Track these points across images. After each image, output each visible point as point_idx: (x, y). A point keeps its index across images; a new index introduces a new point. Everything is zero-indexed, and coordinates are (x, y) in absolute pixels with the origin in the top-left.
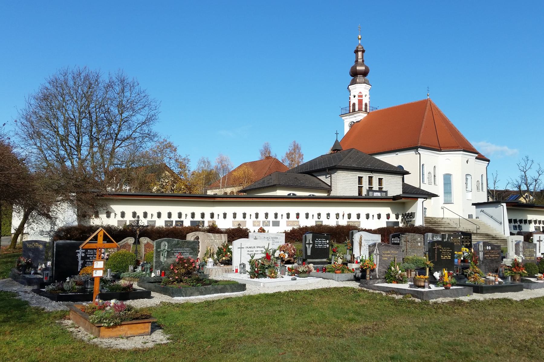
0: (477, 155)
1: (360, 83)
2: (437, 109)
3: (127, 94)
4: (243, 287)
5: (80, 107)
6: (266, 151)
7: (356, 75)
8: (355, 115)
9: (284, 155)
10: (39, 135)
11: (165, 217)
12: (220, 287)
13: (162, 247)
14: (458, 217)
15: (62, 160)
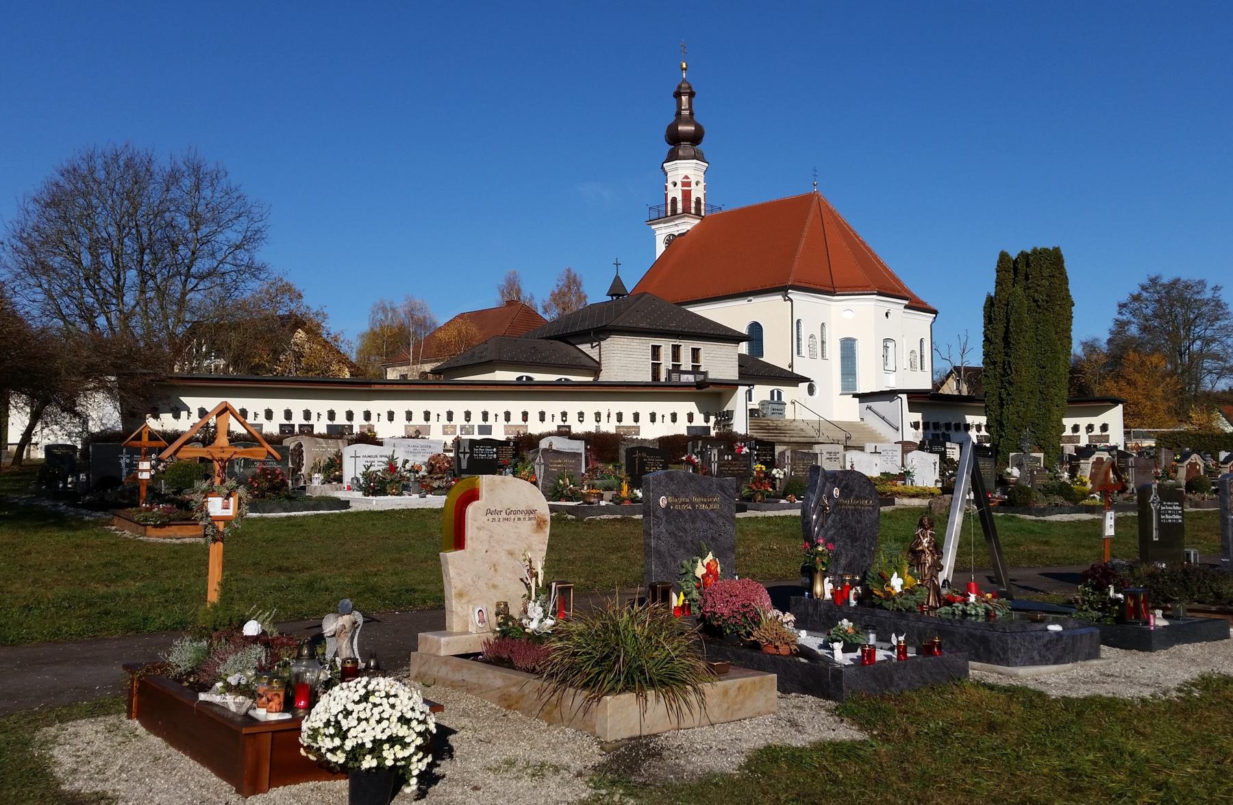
0: (906, 302)
1: (685, 158)
2: (831, 212)
3: (207, 193)
4: (346, 504)
5: (121, 219)
6: (512, 286)
7: (681, 142)
9: (547, 297)
10: (47, 269)
12: (312, 503)
15: (88, 315)
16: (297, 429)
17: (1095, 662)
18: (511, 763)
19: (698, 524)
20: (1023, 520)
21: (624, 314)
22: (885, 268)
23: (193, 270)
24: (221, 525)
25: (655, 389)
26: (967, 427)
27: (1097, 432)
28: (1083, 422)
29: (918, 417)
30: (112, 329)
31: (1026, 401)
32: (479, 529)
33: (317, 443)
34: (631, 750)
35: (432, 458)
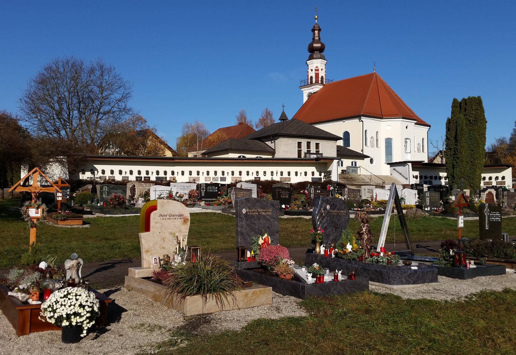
0: (416, 122)
2: (382, 82)
3: (106, 77)
5: (71, 91)
6: (242, 116)
7: (315, 51)
8: (313, 87)
11: (136, 174)
12: (134, 211)
13: (104, 189)
14: (370, 174)
16: (143, 179)
17: (434, 284)
18: (142, 325)
19: (261, 221)
20: (449, 220)
21: (284, 129)
22: (406, 106)
23: (101, 111)
24: (35, 221)
25: (299, 161)
26: (440, 178)
27: (500, 180)
28: (494, 175)
29: (417, 173)
30: (68, 138)
31: (465, 166)
32: (156, 223)
33: (142, 185)
34: (197, 320)
35: (190, 192)
